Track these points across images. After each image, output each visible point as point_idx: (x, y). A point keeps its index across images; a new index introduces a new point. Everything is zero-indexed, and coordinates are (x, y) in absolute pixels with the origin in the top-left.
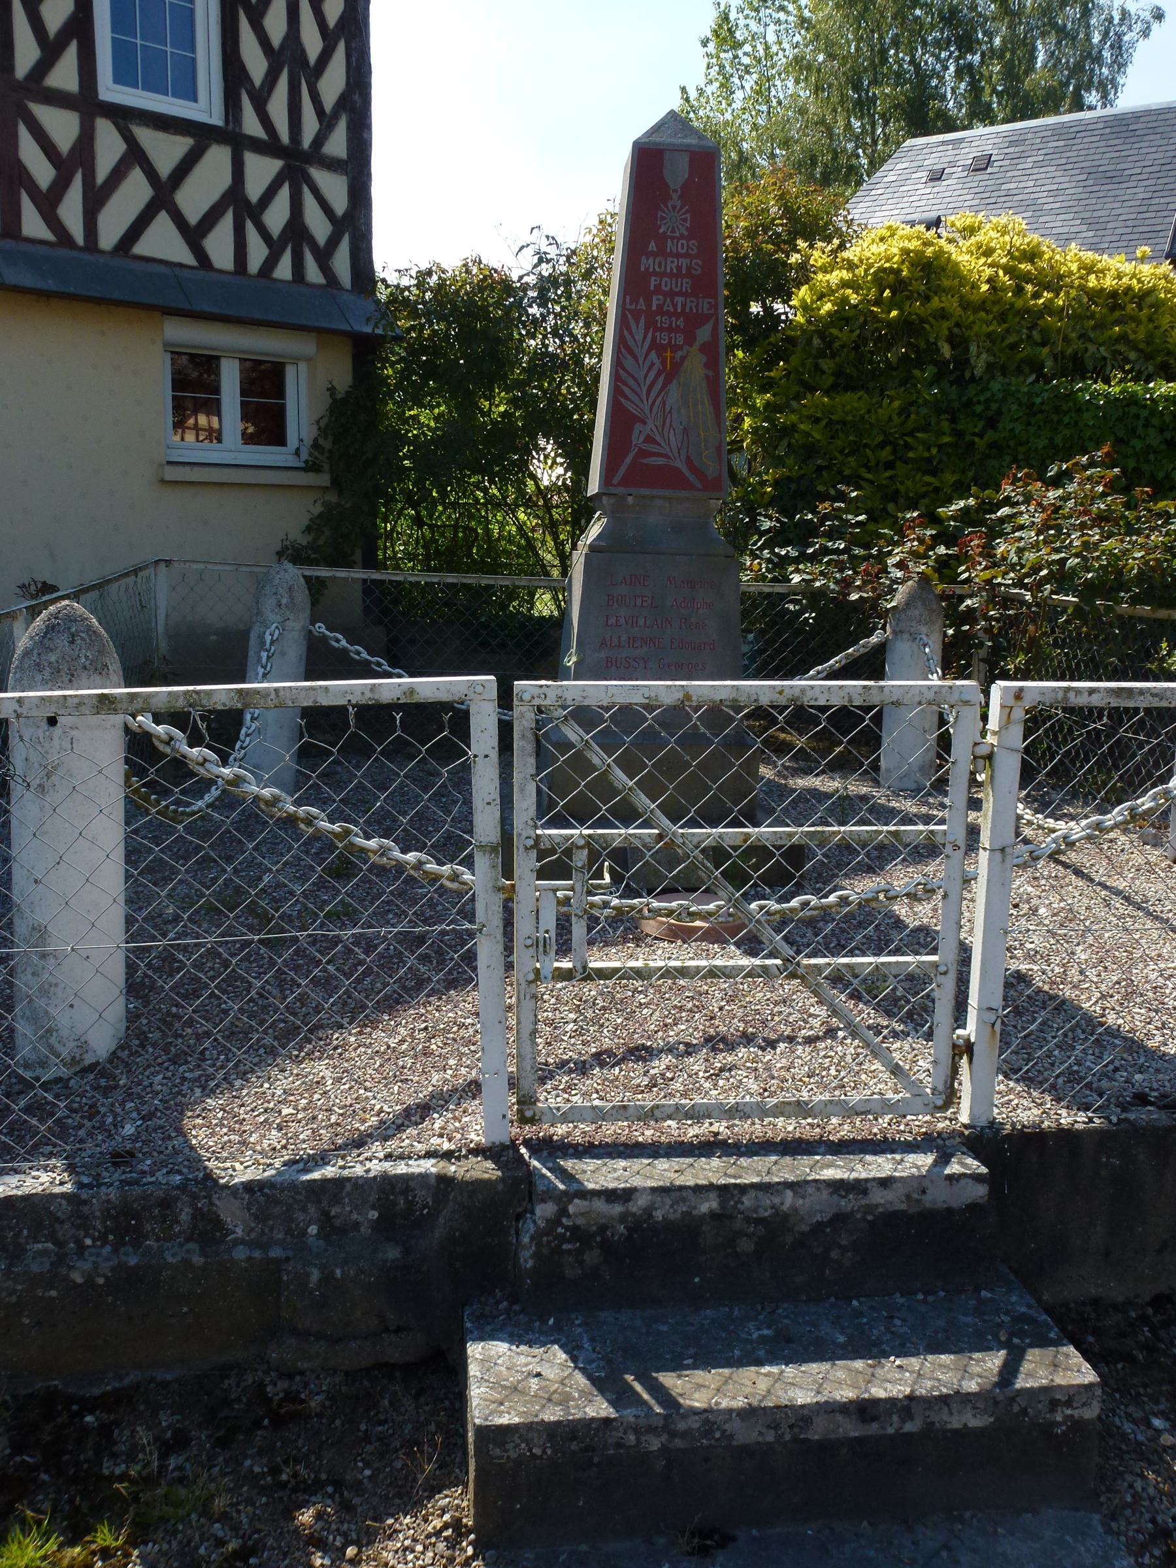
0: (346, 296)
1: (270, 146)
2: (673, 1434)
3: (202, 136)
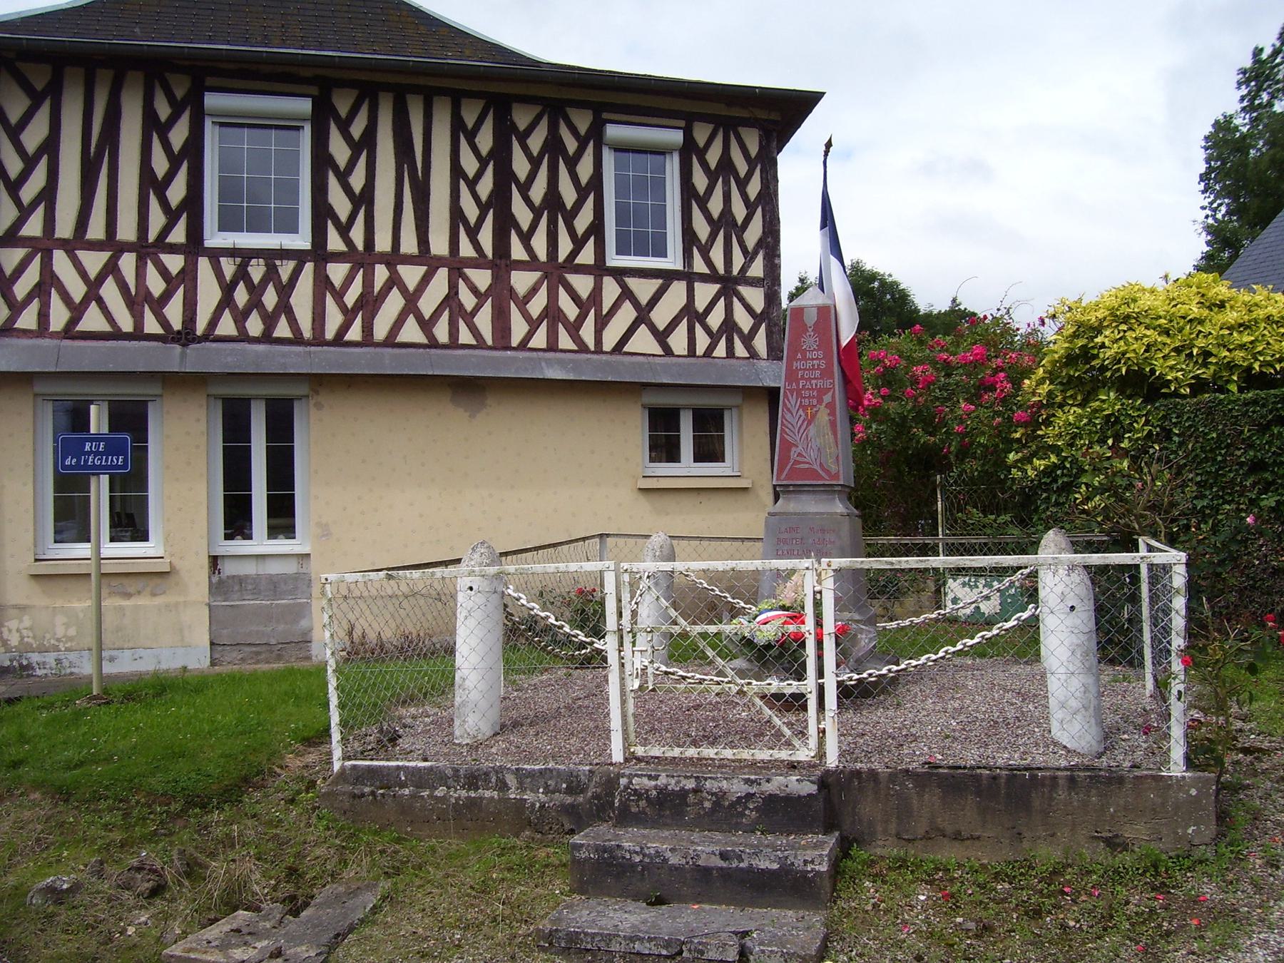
0: (763, 363)
1: (712, 277)
2: (644, 855)
3: (668, 277)
